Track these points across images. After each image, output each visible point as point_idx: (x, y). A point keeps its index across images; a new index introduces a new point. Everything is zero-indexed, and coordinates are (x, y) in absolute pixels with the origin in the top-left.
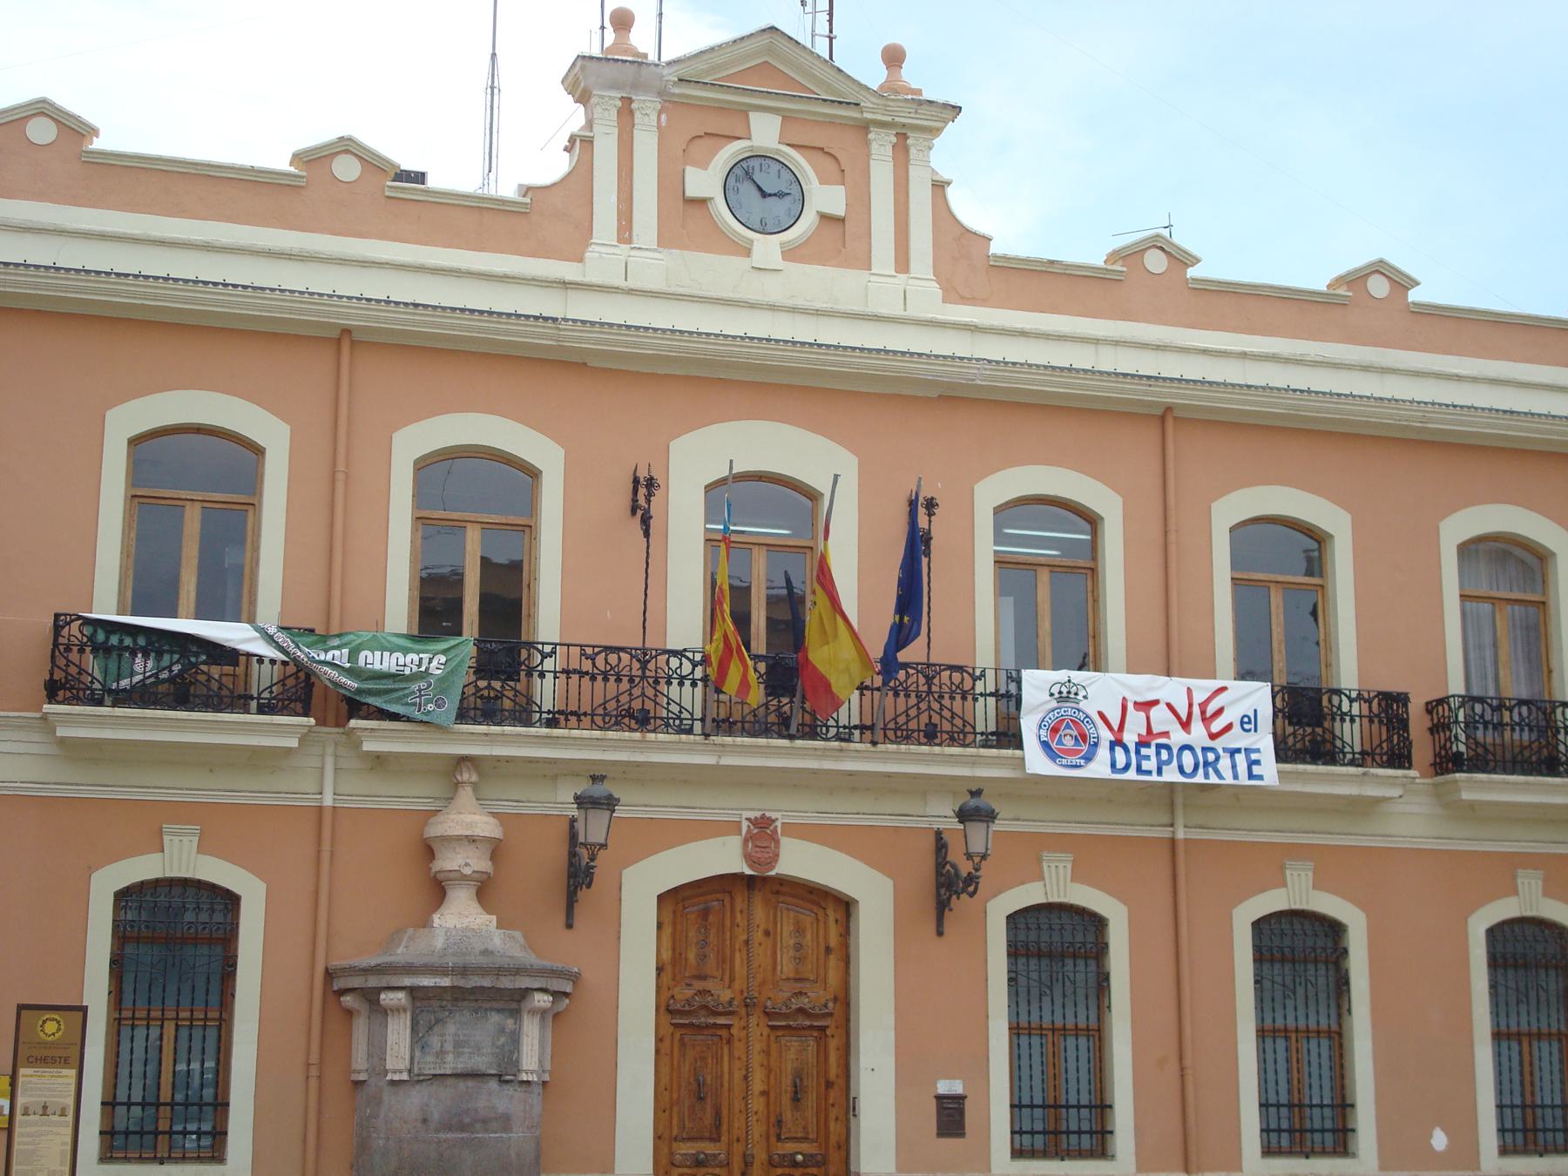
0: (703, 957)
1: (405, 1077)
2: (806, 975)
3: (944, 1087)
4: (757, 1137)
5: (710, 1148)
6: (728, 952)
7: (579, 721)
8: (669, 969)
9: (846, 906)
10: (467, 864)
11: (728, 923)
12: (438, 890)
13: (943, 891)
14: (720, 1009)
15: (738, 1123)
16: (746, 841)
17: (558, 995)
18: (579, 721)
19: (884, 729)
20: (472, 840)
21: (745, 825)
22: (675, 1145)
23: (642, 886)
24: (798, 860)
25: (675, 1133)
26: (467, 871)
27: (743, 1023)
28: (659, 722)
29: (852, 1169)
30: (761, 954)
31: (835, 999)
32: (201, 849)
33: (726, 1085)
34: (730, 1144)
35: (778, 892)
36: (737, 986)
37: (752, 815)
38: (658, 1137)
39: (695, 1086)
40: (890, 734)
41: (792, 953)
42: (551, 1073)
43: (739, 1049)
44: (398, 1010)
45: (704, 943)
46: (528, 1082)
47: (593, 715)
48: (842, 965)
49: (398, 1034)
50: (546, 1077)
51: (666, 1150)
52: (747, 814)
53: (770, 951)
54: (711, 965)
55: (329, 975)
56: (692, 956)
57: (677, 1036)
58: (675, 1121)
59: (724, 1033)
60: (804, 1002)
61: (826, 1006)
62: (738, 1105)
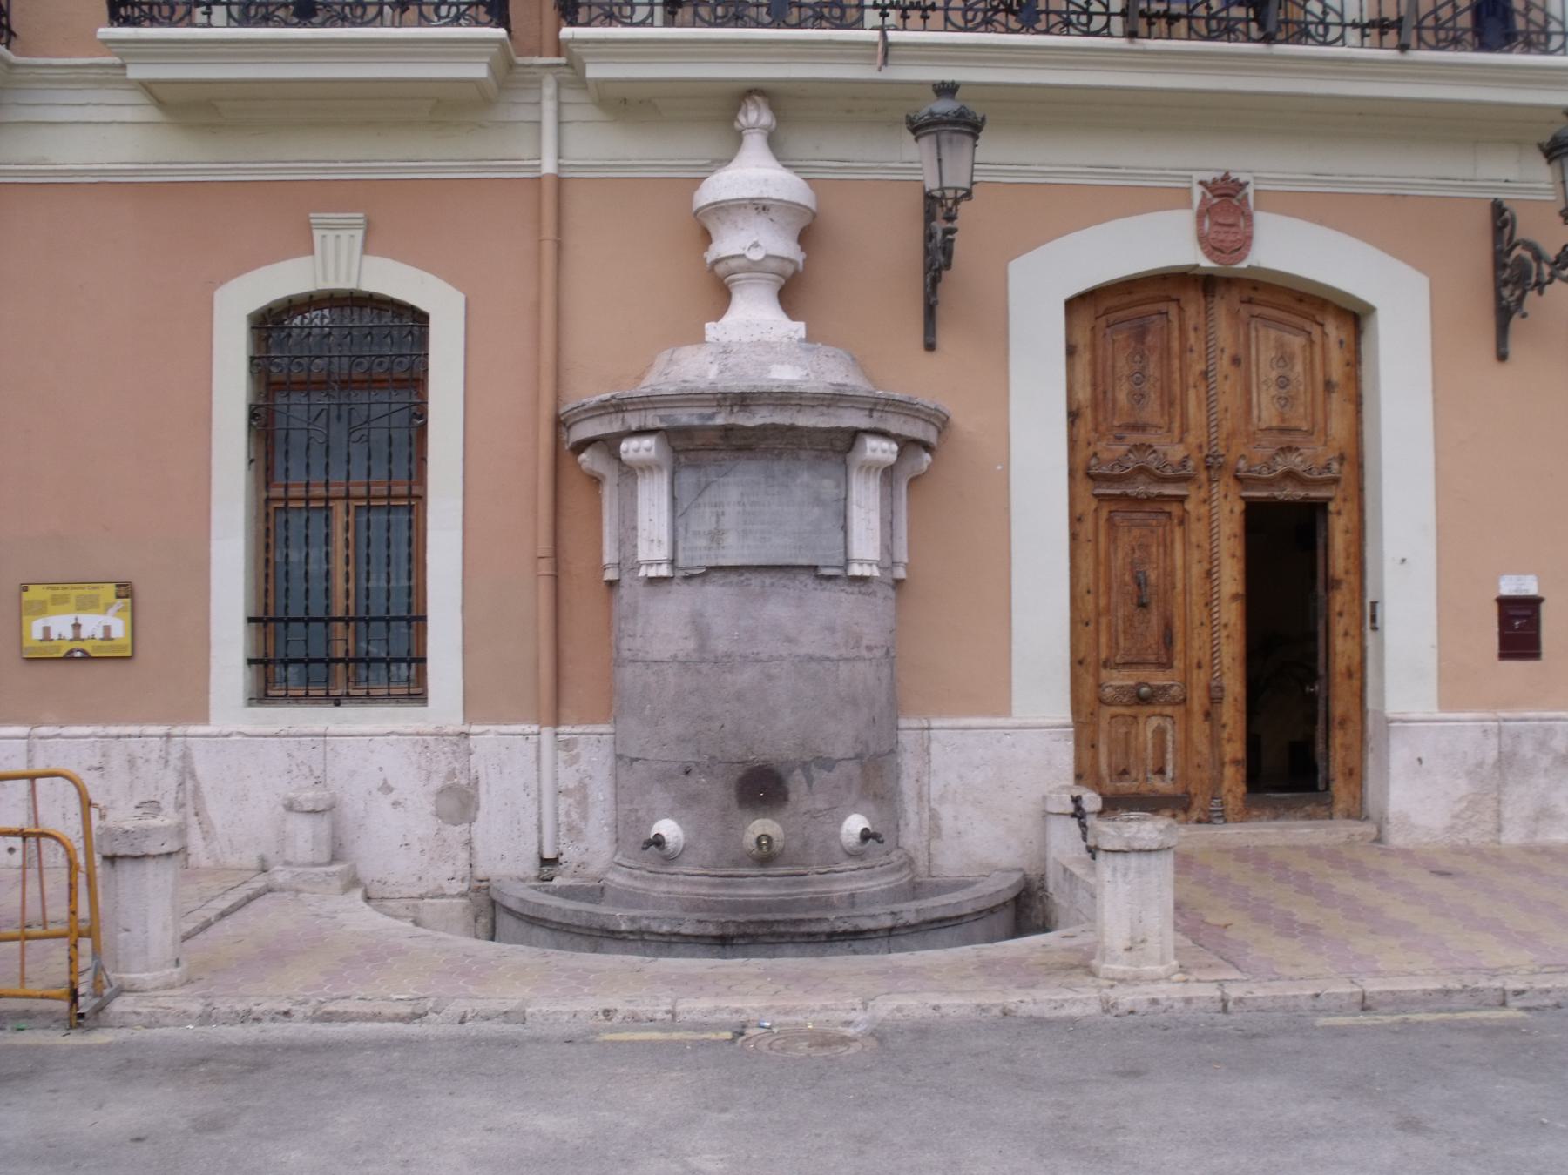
0: (1138, 398)
1: (664, 571)
2: (1293, 424)
3: (1510, 586)
4: (1227, 661)
5: (1159, 679)
6: (1177, 389)
7: (925, 18)
8: (1088, 414)
9: (1355, 316)
10: (756, 245)
11: (1175, 345)
12: (719, 291)
13: (1506, 292)
14: (1169, 472)
15: (1199, 641)
16: (1200, 217)
17: (908, 445)
18: (925, 18)
19: (1419, 27)
20: (761, 206)
21: (1197, 193)
22: (1104, 673)
23: (1038, 287)
24: (1283, 247)
25: (1103, 656)
26: (756, 255)
27: (1203, 494)
28: (1054, 19)
29: (1370, 704)
30: (1228, 393)
31: (1342, 458)
32: (366, 249)
33: (1179, 586)
34: (1187, 670)
35: (1250, 301)
36: (1192, 439)
37: (1208, 177)
38: (1077, 662)
39: (1132, 588)
40: (1428, 36)
41: (1273, 391)
42: (907, 567)
43: (1197, 531)
44: (648, 467)
45: (1139, 377)
46: (863, 580)
47: (946, 9)
48: (1351, 407)
49: (652, 504)
50: (901, 573)
51: (1090, 681)
52: (1198, 176)
53: (1242, 393)
54: (1152, 411)
55: (561, 424)
56: (1122, 397)
57: (1104, 514)
58: (1103, 639)
59: (1174, 509)
60: (1295, 461)
61: (1328, 467)
62: (1198, 613)
